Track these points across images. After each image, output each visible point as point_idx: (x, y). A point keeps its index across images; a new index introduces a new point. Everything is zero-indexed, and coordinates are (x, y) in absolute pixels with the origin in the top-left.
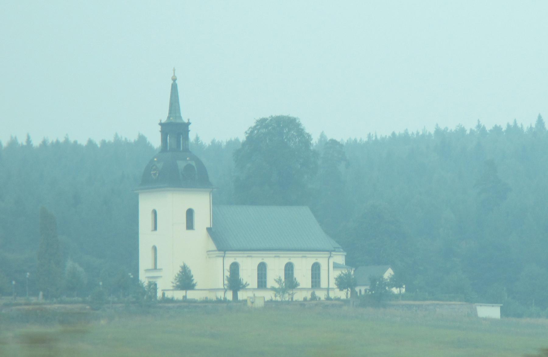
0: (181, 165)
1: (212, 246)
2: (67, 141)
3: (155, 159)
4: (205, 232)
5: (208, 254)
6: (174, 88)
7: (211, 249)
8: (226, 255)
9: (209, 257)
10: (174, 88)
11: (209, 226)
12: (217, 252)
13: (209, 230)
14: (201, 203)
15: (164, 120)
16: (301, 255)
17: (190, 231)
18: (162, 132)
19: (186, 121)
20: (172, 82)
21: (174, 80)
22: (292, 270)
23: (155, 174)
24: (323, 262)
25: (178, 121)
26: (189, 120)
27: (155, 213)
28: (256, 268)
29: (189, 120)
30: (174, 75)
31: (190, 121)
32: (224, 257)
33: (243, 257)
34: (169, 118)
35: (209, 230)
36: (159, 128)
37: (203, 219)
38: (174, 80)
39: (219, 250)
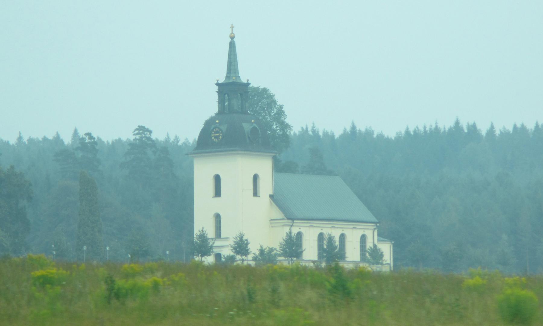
0: (247, 127)
1: (277, 214)
2: (407, 132)
3: (217, 121)
4: (268, 199)
5: (271, 223)
6: (232, 45)
7: (278, 218)
8: (294, 224)
9: (272, 227)
10: (232, 45)
11: (271, 194)
12: (287, 221)
13: (271, 197)
14: (263, 166)
15: (222, 80)
16: (330, 226)
17: (256, 198)
18: (220, 92)
19: (245, 82)
20: (230, 40)
21: (232, 38)
22: (301, 240)
23: (217, 137)
24: (347, 232)
25: (239, 81)
26: (248, 80)
27: (217, 179)
28: (317, 239)
29: (248, 80)
30: (232, 33)
31: (250, 82)
32: (291, 226)
33: (307, 226)
34: (228, 77)
35: (271, 197)
36: (216, 88)
37: (266, 186)
38: (232, 38)
39: (288, 219)
